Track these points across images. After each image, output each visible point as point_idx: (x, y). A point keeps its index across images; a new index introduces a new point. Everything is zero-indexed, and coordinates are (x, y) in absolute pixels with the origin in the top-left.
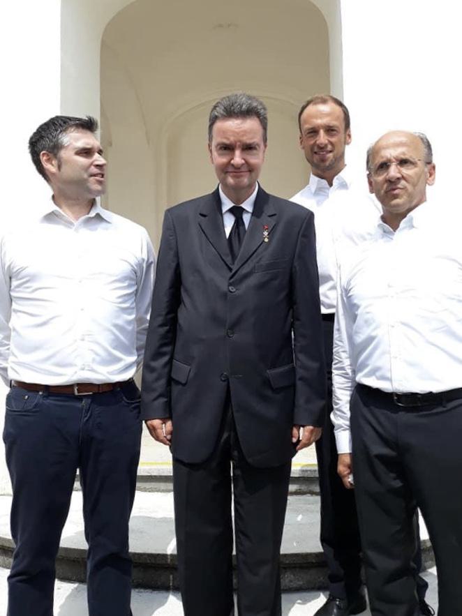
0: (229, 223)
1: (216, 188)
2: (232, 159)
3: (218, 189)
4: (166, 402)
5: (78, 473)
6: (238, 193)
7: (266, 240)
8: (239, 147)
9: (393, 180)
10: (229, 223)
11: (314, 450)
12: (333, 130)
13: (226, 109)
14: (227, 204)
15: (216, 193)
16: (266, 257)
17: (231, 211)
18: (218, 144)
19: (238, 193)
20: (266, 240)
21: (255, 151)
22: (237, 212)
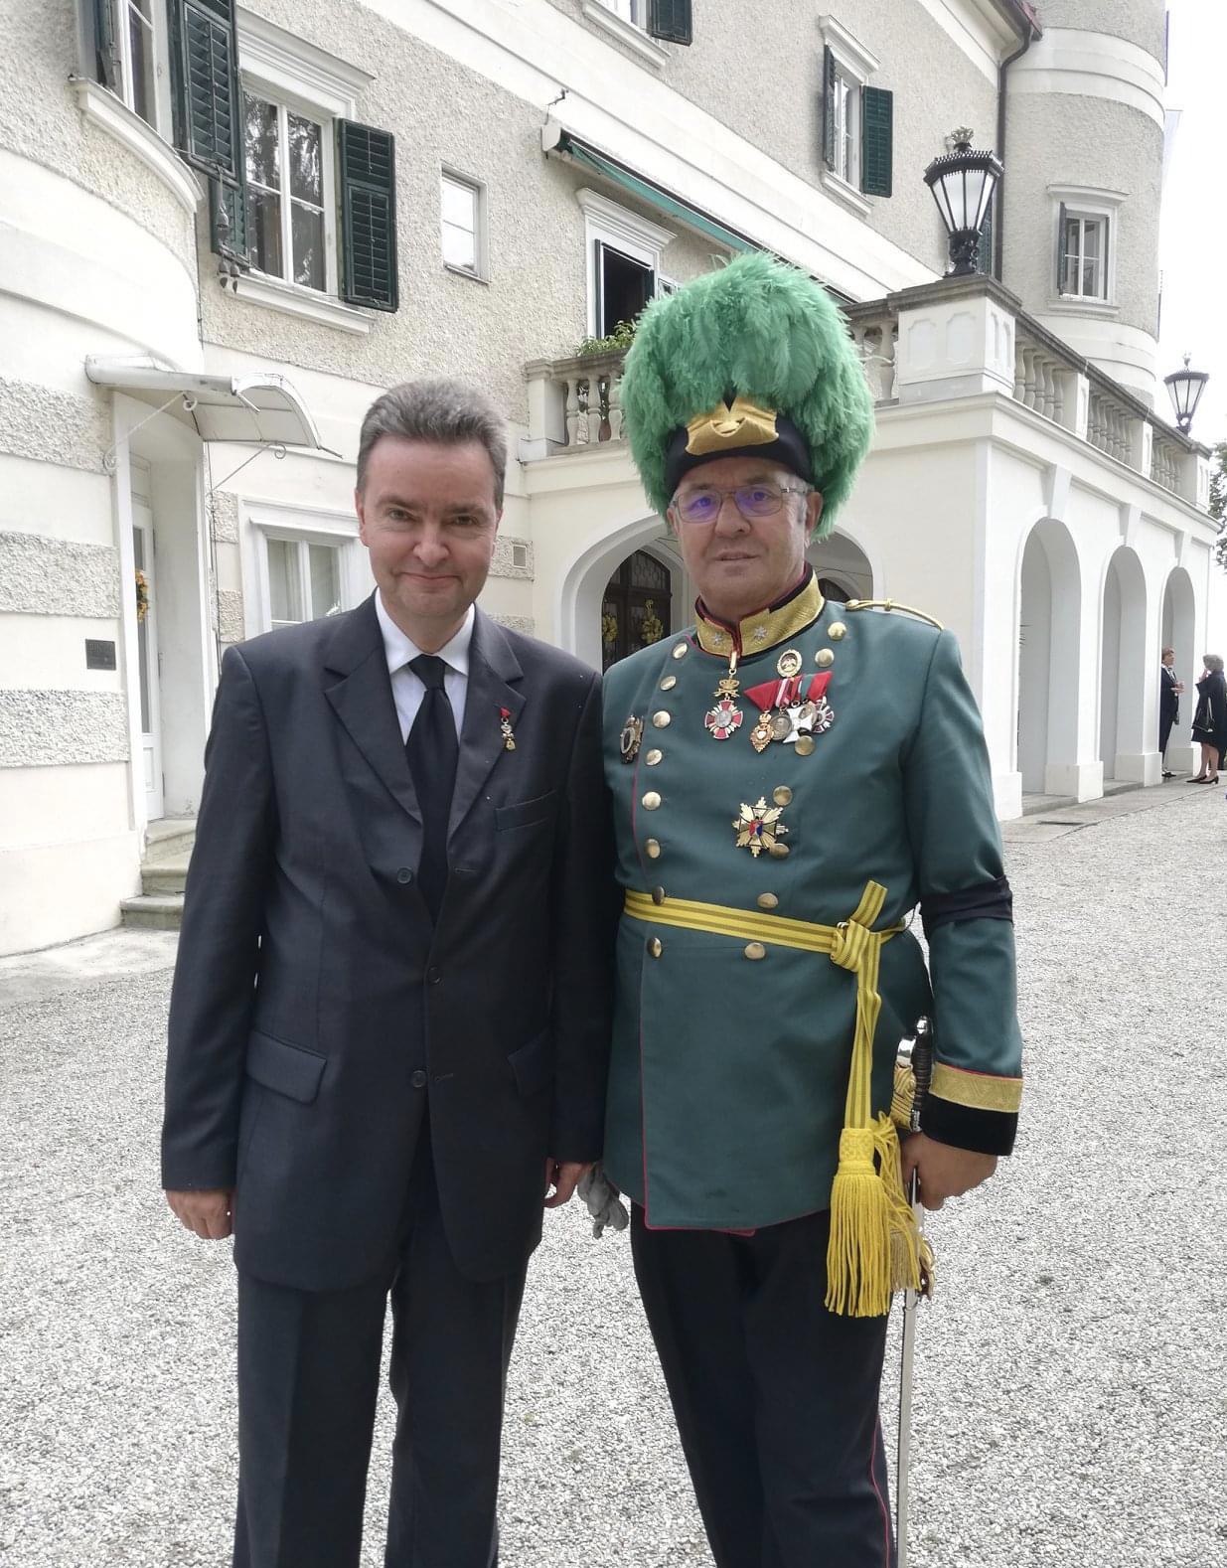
0: (409, 700)
1: (370, 594)
2: (416, 544)
3: (372, 599)
4: (993, 446)
5: (389, 1297)
6: (435, 624)
7: (511, 745)
8: (435, 515)
9: (762, 402)
10: (409, 700)
11: (628, 1236)
12: (658, 68)
13: (404, 416)
14: (400, 652)
15: (370, 604)
16: (515, 785)
17: (413, 667)
18: (382, 502)
19: (435, 624)
20: (511, 745)
21: (474, 530)
22: (428, 669)
